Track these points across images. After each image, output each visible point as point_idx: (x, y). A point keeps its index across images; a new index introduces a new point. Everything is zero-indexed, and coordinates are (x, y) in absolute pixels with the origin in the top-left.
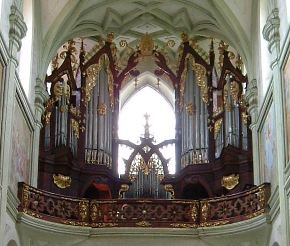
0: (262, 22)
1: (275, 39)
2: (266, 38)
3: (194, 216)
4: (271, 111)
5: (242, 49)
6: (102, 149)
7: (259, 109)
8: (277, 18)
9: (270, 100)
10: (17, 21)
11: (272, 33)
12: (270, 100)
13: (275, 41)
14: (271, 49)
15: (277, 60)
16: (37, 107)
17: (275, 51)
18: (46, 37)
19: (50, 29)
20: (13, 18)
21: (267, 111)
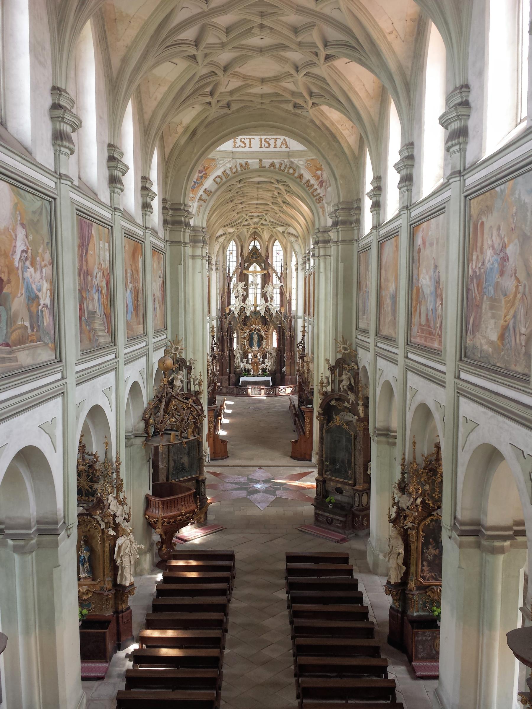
18: (168, 158)
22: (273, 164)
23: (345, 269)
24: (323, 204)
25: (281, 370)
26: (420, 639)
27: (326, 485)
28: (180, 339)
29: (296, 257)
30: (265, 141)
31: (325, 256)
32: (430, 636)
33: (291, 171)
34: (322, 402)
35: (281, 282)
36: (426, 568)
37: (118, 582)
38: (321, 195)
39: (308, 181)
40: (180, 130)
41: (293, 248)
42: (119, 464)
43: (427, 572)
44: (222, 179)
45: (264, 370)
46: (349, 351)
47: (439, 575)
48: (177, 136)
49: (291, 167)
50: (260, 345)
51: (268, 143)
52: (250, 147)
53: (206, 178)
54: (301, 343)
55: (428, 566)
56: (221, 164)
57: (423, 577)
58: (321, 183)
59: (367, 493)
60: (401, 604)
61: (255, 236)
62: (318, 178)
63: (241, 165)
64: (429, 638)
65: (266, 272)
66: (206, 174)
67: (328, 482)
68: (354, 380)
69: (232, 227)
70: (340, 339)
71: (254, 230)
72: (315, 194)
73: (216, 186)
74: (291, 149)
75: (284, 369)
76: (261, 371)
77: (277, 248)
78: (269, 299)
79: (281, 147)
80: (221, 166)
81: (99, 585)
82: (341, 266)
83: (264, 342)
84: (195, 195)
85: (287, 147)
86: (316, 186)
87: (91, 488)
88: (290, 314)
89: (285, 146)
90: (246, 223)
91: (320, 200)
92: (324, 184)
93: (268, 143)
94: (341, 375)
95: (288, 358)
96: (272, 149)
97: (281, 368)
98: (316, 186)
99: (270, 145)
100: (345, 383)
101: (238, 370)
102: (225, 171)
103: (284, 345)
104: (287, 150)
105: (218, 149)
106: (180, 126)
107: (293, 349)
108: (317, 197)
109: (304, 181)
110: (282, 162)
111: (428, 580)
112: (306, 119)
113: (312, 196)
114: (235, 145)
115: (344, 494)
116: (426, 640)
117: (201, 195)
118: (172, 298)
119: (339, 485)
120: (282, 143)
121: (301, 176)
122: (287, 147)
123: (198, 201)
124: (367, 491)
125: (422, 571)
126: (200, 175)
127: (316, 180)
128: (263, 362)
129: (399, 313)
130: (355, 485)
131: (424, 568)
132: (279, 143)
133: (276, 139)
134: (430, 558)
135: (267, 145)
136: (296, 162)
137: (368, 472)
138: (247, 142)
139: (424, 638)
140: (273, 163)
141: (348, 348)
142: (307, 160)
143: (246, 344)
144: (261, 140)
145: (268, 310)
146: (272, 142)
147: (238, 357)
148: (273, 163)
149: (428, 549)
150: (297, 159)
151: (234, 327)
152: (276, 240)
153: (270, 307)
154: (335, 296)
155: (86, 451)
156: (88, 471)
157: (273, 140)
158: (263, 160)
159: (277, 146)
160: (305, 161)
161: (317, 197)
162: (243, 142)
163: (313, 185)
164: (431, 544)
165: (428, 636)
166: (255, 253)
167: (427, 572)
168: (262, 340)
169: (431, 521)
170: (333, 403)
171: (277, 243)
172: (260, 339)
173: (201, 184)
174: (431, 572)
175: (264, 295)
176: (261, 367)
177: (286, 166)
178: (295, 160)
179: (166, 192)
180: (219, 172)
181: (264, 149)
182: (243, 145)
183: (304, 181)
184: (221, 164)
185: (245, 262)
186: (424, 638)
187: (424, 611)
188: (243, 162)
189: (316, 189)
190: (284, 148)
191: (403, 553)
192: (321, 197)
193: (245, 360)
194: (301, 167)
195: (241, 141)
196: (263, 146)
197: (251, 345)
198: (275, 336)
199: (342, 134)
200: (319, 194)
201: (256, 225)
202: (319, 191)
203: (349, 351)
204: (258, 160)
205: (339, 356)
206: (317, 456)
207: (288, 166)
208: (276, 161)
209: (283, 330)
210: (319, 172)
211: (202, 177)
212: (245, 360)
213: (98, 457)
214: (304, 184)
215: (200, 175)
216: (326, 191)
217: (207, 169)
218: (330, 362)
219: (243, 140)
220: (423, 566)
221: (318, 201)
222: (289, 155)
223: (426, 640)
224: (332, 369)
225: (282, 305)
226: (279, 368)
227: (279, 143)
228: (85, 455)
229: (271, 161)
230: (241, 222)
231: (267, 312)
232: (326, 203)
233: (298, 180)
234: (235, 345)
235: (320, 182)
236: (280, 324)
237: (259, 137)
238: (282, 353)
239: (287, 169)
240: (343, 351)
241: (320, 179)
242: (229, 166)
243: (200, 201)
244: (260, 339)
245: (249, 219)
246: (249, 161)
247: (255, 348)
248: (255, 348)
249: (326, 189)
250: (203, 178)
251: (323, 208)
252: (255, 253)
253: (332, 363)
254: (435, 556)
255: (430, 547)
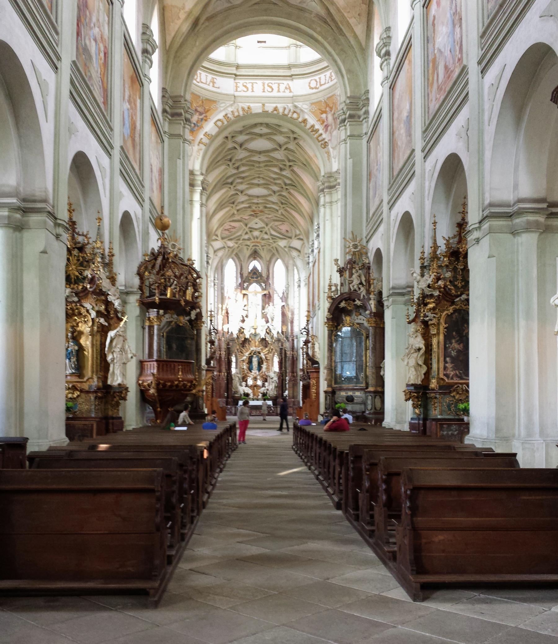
0: (376, 40)
1: (386, 57)
2: (379, 55)
3: (233, 412)
4: (381, 124)
5: (356, 57)
6: (204, 82)
7: (370, 119)
8: (389, 37)
9: (408, 45)
10: (149, 40)
11: (383, 51)
12: (408, 45)
13: (386, 60)
14: (383, 67)
15: (387, 78)
16: (144, 58)
17: (385, 69)
18: (169, 47)
19: (174, 38)
20: (145, 37)
21: (401, 66)
22: (276, 109)
23: (354, 165)
24: (328, 149)
25: (283, 395)
26: (445, 433)
27: (336, 396)
28: (178, 238)
29: (299, 273)
30: (269, 86)
31: (331, 202)
32: (456, 431)
33: (295, 116)
34: (330, 307)
35: (282, 302)
36: (449, 365)
37: (109, 382)
38: (326, 140)
39: (313, 126)
40: (183, 16)
41: (295, 265)
42: (113, 255)
43: (451, 369)
44: (223, 123)
45: (264, 395)
46: (359, 247)
47: (464, 373)
48: (179, 22)
49: (295, 112)
50: (260, 368)
51: (271, 87)
52: (253, 91)
53: (206, 120)
54: (305, 328)
55: (452, 363)
56: (222, 107)
57: (447, 375)
58: (326, 127)
59: (381, 397)
60: (422, 411)
61: (255, 255)
62: (323, 122)
63: (243, 109)
64: (456, 433)
65: (266, 292)
66: (206, 116)
67: (338, 393)
68: (365, 277)
69: (231, 240)
70: (349, 236)
71: (254, 248)
72: (320, 138)
73: (217, 130)
74: (295, 94)
75: (286, 393)
76: (261, 395)
77: (279, 267)
78: (270, 320)
79: (284, 92)
80: (222, 109)
81: (88, 383)
82: (350, 162)
83: (264, 366)
84: (195, 137)
85: (291, 92)
86: (321, 131)
87: (81, 274)
88: (292, 333)
89: (288, 91)
90: (246, 237)
91: (325, 145)
92: (329, 128)
93: (271, 87)
94: (351, 275)
95: (289, 381)
96: (275, 94)
97: (283, 392)
98: (321, 131)
99: (273, 89)
100: (356, 282)
101: (236, 395)
102: (226, 115)
103: (285, 368)
104: (291, 95)
105: (220, 54)
106: (182, 11)
107: (295, 370)
108: (323, 142)
109: (308, 126)
110: (286, 107)
111: (452, 379)
112: (311, 14)
113: (317, 141)
114: (237, 89)
115: (355, 401)
116: (452, 435)
117: (201, 139)
118: (169, 193)
119: (350, 393)
120: (286, 88)
121: (305, 121)
122: (291, 92)
123: (198, 145)
124: (381, 395)
125: (445, 368)
126: (201, 117)
127: (321, 124)
128: (263, 385)
129: (415, 128)
130: (367, 388)
131: (447, 365)
132: (282, 87)
133: (279, 84)
134: (454, 353)
135: (270, 90)
136: (299, 106)
137: (382, 373)
138: (249, 86)
139: (450, 433)
140: (276, 107)
141: (359, 244)
142: (312, 104)
143: (245, 367)
144: (264, 84)
145: (268, 332)
146: (275, 87)
147: (236, 381)
148: (276, 107)
149: (451, 343)
150: (301, 103)
151: (232, 349)
152: (278, 259)
153: (271, 327)
154: (344, 197)
155: (77, 230)
156: (79, 256)
157: (277, 85)
158: (266, 105)
159: (280, 90)
160: (309, 105)
161: (323, 142)
162: (245, 86)
163: (317, 131)
164: (455, 338)
165: (454, 430)
166: (255, 273)
167: (451, 369)
168: (263, 364)
169: (455, 311)
170: (343, 304)
171: (279, 262)
172: (260, 363)
173: (201, 127)
174: (455, 370)
175: (264, 316)
176: (262, 390)
177: (290, 110)
178: (299, 105)
179: (166, 82)
180: (220, 116)
181: (267, 94)
182: (245, 90)
183: (308, 126)
184: (222, 107)
185: (244, 282)
186: (450, 433)
187: (449, 414)
188: (245, 106)
189: (321, 134)
190: (287, 94)
191: (424, 348)
192: (326, 142)
193: (244, 384)
194: (306, 111)
195: (244, 86)
196: (266, 90)
197: (250, 369)
198: (276, 360)
199: (349, 23)
200: (324, 139)
201: (256, 240)
202: (324, 136)
203: (359, 247)
204: (261, 104)
205: (349, 257)
206: (326, 382)
207: (292, 111)
208: (279, 106)
209: (285, 351)
210: (324, 116)
211: (202, 119)
212: (244, 384)
213: (90, 238)
214: (309, 129)
215: (201, 117)
216: (331, 136)
217: (208, 111)
218: (339, 262)
219: (245, 84)
220: (446, 362)
221: (323, 146)
222: (294, 99)
223: (452, 435)
224: (341, 271)
225: (284, 322)
226: (280, 392)
227: (282, 87)
228: (76, 236)
229: (274, 105)
230: (241, 235)
231: (268, 334)
232: (332, 148)
233: (303, 124)
234: (234, 370)
235: (326, 126)
236: (282, 346)
237: (262, 81)
238: (284, 376)
239: (291, 113)
240: (353, 250)
241: (325, 123)
242: (230, 109)
243: (200, 145)
244: (260, 363)
245: (249, 232)
246: (252, 105)
247: (255, 372)
248: (255, 372)
249: (331, 133)
250: (203, 121)
251: (328, 153)
252: (255, 273)
253: (341, 264)
254: (459, 351)
255: (453, 341)
